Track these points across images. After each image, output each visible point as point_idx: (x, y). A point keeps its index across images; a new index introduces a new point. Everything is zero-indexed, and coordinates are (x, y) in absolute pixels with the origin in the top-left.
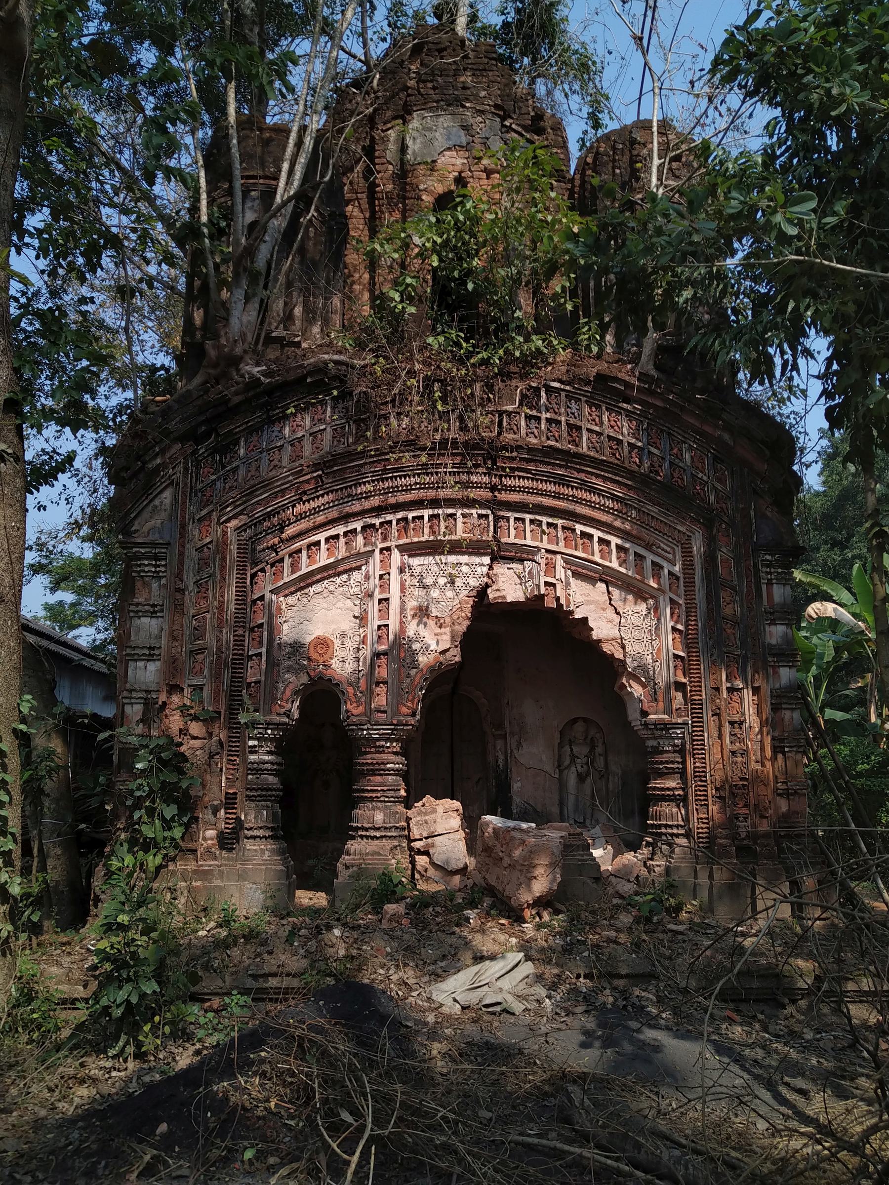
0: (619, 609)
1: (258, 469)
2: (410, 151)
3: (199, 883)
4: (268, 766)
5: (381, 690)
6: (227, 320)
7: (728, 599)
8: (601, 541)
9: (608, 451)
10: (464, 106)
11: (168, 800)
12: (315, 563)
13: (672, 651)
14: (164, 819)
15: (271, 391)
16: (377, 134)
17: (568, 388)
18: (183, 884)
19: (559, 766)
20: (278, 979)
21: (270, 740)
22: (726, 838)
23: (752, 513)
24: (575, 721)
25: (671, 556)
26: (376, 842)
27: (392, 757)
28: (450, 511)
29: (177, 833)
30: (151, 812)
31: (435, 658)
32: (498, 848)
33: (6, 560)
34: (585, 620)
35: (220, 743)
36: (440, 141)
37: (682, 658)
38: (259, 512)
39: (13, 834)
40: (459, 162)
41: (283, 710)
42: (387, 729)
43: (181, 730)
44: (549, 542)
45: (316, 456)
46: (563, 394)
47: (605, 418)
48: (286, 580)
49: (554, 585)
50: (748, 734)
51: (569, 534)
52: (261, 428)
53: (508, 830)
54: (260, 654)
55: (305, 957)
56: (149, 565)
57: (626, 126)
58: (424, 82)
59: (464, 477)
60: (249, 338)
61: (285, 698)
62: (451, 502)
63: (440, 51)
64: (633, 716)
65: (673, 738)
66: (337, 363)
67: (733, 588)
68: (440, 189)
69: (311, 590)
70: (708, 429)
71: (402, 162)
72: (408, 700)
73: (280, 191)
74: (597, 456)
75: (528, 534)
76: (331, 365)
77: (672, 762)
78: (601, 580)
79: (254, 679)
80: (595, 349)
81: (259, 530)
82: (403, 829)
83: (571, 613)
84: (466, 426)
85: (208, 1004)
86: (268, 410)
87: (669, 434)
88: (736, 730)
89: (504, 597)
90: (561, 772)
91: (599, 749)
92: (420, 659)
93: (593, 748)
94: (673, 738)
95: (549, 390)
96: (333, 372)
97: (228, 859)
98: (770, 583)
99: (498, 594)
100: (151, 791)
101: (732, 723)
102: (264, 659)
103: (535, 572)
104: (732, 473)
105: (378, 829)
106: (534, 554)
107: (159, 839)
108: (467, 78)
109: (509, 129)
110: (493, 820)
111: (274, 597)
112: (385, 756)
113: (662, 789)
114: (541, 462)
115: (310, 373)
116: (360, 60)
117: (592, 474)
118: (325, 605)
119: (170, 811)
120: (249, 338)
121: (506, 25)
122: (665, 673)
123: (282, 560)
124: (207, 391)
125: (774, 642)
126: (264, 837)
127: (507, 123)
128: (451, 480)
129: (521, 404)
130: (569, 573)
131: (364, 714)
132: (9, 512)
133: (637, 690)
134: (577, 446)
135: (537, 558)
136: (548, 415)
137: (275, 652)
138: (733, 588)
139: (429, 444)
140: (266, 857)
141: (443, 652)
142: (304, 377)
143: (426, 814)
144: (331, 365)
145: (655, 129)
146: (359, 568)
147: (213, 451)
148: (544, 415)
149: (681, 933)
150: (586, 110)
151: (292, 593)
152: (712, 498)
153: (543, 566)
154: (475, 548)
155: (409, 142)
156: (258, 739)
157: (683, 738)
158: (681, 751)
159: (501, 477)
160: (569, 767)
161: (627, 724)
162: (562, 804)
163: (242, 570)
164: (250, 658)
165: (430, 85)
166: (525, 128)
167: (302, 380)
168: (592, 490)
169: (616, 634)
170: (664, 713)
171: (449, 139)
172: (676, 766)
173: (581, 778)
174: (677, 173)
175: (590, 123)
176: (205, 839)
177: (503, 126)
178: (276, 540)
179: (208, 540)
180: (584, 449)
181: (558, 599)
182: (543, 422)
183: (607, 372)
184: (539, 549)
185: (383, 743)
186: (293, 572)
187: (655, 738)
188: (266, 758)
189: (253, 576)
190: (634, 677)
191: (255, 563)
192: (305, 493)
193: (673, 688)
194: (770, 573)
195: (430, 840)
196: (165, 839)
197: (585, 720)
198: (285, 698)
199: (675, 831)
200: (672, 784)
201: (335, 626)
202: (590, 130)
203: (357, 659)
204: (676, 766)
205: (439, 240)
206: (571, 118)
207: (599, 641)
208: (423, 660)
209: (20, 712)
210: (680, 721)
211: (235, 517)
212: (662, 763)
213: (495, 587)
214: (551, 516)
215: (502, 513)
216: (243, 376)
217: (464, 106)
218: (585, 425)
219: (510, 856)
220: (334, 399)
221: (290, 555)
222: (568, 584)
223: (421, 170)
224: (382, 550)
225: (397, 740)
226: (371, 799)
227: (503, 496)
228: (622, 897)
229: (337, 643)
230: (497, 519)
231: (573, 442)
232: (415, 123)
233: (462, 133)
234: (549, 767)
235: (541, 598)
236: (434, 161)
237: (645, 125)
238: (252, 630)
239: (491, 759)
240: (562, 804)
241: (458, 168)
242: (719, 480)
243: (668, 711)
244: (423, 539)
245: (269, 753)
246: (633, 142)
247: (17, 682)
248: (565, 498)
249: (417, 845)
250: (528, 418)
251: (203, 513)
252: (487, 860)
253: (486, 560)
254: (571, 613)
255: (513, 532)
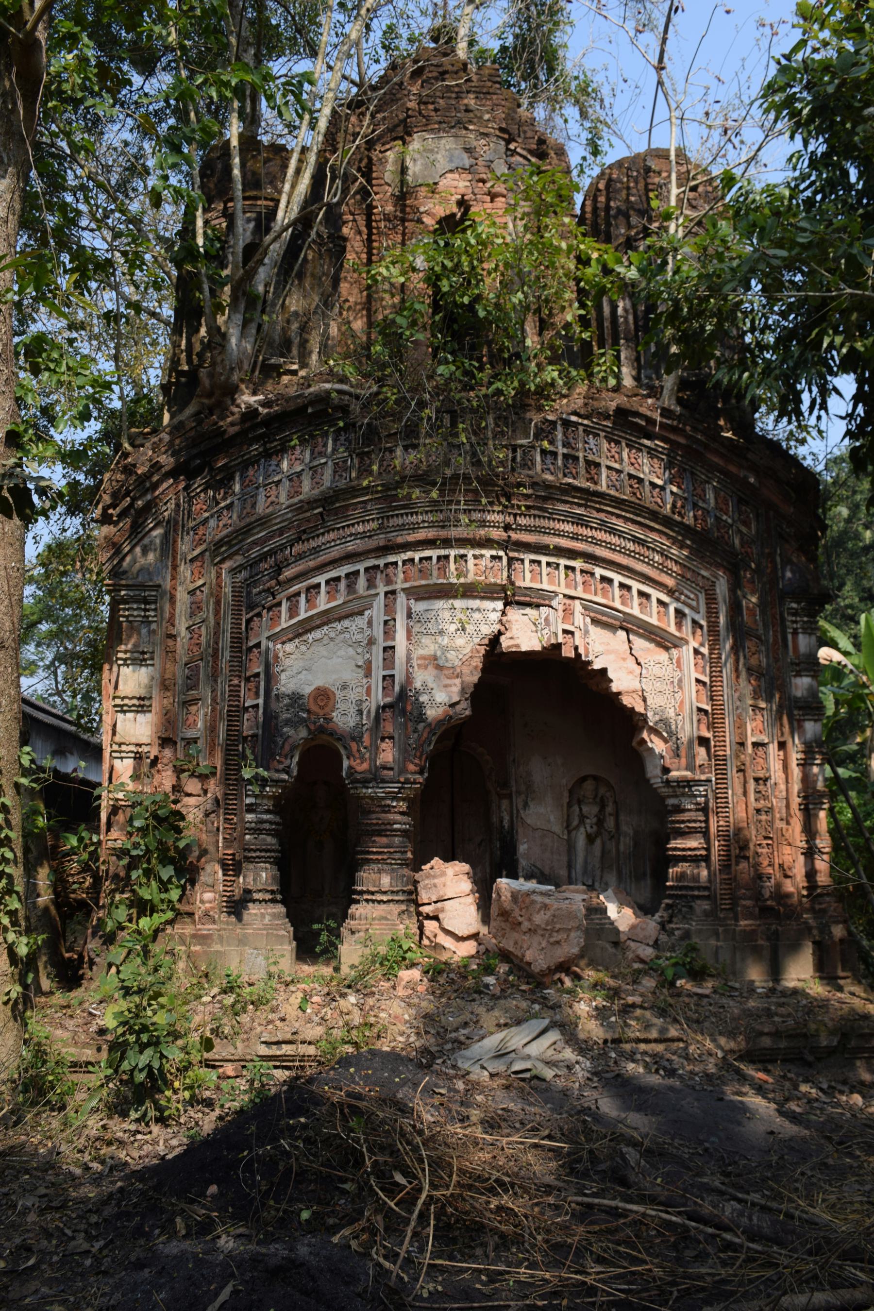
0: (640, 660)
1: (254, 505)
2: (410, 172)
3: (198, 948)
4: (267, 826)
5: (387, 745)
6: (223, 347)
7: (753, 649)
8: (622, 586)
9: (628, 490)
10: (466, 129)
11: (164, 860)
12: (315, 607)
13: (696, 704)
14: (161, 881)
15: (269, 421)
17: (586, 422)
18: (183, 948)
19: (567, 827)
21: (269, 797)
22: (750, 898)
23: (778, 559)
24: (584, 779)
25: (694, 603)
27: (398, 817)
28: (462, 551)
29: (175, 894)
30: (148, 873)
32: (517, 913)
33: (6, 603)
34: (604, 671)
35: (217, 800)
36: (442, 163)
37: (706, 712)
38: (254, 553)
39: (17, 893)
41: (281, 767)
43: (174, 787)
45: (316, 492)
46: (581, 428)
47: (625, 455)
49: (572, 633)
50: (773, 791)
51: (587, 577)
52: (257, 462)
53: (528, 894)
54: (256, 706)
56: (138, 609)
58: (426, 103)
59: (477, 516)
60: (246, 366)
61: (284, 752)
62: (463, 542)
64: (653, 772)
65: (695, 796)
66: (339, 392)
68: (441, 211)
69: (310, 637)
70: (733, 469)
71: (403, 182)
72: (415, 756)
73: (280, 214)
74: (617, 494)
75: (545, 578)
77: (695, 821)
78: (622, 628)
79: (250, 733)
80: (612, 382)
81: (254, 571)
84: (479, 461)
85: (221, 1070)
86: (265, 444)
87: (692, 473)
88: (761, 787)
89: (518, 646)
90: (569, 832)
91: (610, 809)
92: (429, 712)
93: (603, 807)
94: (695, 796)
95: (567, 424)
96: (336, 401)
97: (228, 923)
98: (795, 633)
99: (511, 642)
100: (148, 851)
101: (757, 780)
102: (261, 711)
103: (551, 618)
104: (757, 516)
105: (385, 893)
106: (551, 599)
107: (156, 901)
108: (470, 101)
109: (514, 152)
110: (503, 883)
111: (271, 645)
112: (391, 816)
113: (684, 850)
115: (311, 403)
116: (353, 82)
118: (325, 653)
119: (166, 873)
120: (246, 366)
121: (504, 49)
123: (279, 604)
124: (200, 423)
125: (799, 694)
127: (512, 146)
128: (464, 519)
129: (537, 437)
130: (588, 620)
133: (658, 745)
134: (596, 483)
135: (554, 603)
136: (565, 451)
137: (274, 705)
140: (267, 920)
141: (453, 705)
142: (305, 407)
146: (361, 613)
148: (561, 450)
149: (707, 996)
150: (585, 135)
151: (290, 640)
152: (737, 542)
154: (489, 592)
155: (408, 162)
156: (256, 796)
157: (706, 796)
158: (705, 810)
159: (515, 515)
160: (577, 827)
161: (644, 781)
162: (570, 866)
164: (246, 709)
165: (431, 107)
166: (530, 152)
168: (612, 531)
169: (637, 686)
170: (687, 769)
171: (451, 161)
172: (697, 825)
173: (590, 839)
174: (694, 203)
177: (508, 149)
179: (201, 582)
180: (603, 487)
181: (576, 648)
182: (560, 458)
184: (556, 594)
186: (291, 617)
187: (676, 796)
189: (248, 621)
190: (654, 731)
192: (304, 531)
193: (696, 743)
194: (796, 622)
195: (439, 905)
196: (162, 901)
197: (595, 778)
198: (284, 752)
199: (696, 893)
201: (334, 677)
203: (360, 712)
204: (697, 825)
206: (572, 144)
207: (619, 693)
208: (431, 713)
209: (21, 765)
210: (703, 777)
211: (229, 557)
212: (683, 822)
214: (569, 558)
215: (515, 554)
216: (238, 406)
217: (466, 129)
218: (604, 462)
219: (530, 920)
222: (587, 632)
223: (423, 192)
224: (386, 593)
225: (403, 799)
226: (377, 861)
227: (515, 536)
228: (642, 961)
229: (339, 695)
230: (511, 560)
231: (591, 479)
232: (416, 144)
233: (465, 156)
234: (557, 828)
235: (558, 647)
236: (436, 184)
237: (662, 155)
238: (248, 680)
239: (495, 819)
240: (570, 866)
243: (690, 767)
244: (430, 582)
246: (648, 170)
247: (16, 734)
248: (584, 539)
249: (425, 909)
250: (544, 452)
251: (196, 553)
252: (503, 925)
253: (499, 605)
254: (589, 663)
255: (528, 575)
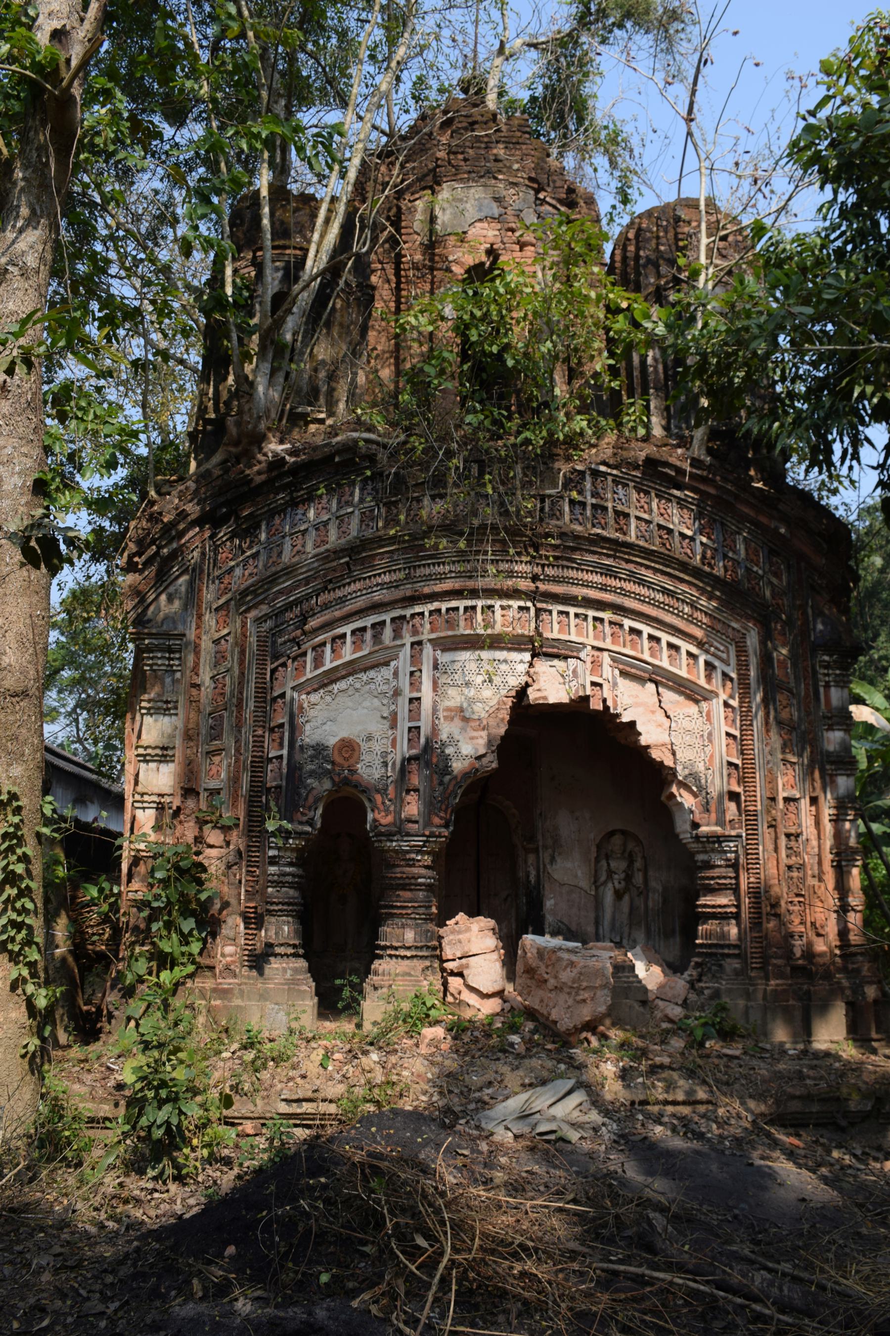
0: (669, 713)
1: (280, 554)
2: (439, 221)
3: (218, 1002)
4: (289, 879)
5: (412, 798)
6: (251, 395)
7: (785, 702)
8: (651, 637)
9: (658, 541)
10: (496, 178)
11: (186, 913)
12: (340, 657)
13: (726, 758)
14: (182, 933)
15: (295, 470)
16: (404, 204)
17: (615, 472)
20: (314, 1105)
21: (292, 850)
24: (612, 834)
25: (724, 656)
26: (406, 962)
27: (423, 871)
29: (195, 947)
30: (168, 925)
31: (471, 764)
32: (543, 969)
34: (633, 724)
35: (239, 852)
38: (280, 602)
39: (37, 944)
40: (491, 233)
41: (305, 819)
42: (418, 841)
43: (196, 838)
44: (596, 638)
46: (610, 478)
47: (654, 505)
48: (309, 675)
49: (600, 685)
51: (616, 629)
52: (284, 511)
54: (280, 757)
55: (341, 1082)
56: (162, 658)
57: (668, 204)
58: (455, 153)
59: (504, 566)
60: (273, 415)
63: (472, 124)
64: (682, 828)
65: (726, 852)
66: (367, 441)
67: (790, 691)
68: (470, 260)
69: (336, 687)
70: (764, 520)
71: (432, 231)
72: (440, 809)
74: (646, 545)
75: (573, 629)
76: (361, 443)
77: (725, 878)
78: (651, 680)
80: (641, 432)
82: (434, 948)
83: (618, 716)
84: (507, 511)
85: (240, 1128)
86: (291, 493)
87: (722, 524)
89: (545, 698)
90: (597, 888)
91: (638, 864)
93: (631, 862)
94: (726, 852)
95: (595, 474)
96: (363, 451)
97: (249, 977)
98: (827, 686)
99: (538, 694)
100: (169, 903)
101: (788, 836)
102: (285, 762)
103: (580, 670)
104: (789, 567)
105: (409, 948)
106: (579, 650)
107: (177, 954)
108: (500, 151)
109: (543, 202)
111: (295, 695)
112: (415, 870)
113: (713, 907)
114: (587, 551)
115: (338, 452)
116: (383, 132)
117: (641, 565)
118: (350, 704)
119: (188, 925)
120: (273, 415)
121: (533, 99)
122: (717, 781)
123: (304, 654)
125: (831, 748)
126: (286, 955)
127: (541, 196)
128: (492, 569)
129: (565, 486)
130: (617, 672)
131: (394, 824)
132: (35, 598)
133: (687, 800)
134: (625, 534)
135: (582, 655)
136: (594, 501)
138: (790, 691)
139: (467, 530)
141: (479, 758)
142: (331, 457)
143: (459, 932)
144: (361, 443)
145: (702, 207)
146: (387, 664)
147: (233, 536)
148: (590, 500)
149: (737, 1058)
150: (615, 184)
151: (315, 690)
152: (768, 593)
153: (589, 665)
154: (517, 643)
155: (438, 212)
156: (279, 849)
158: (735, 866)
159: (543, 566)
160: (605, 883)
162: (597, 923)
163: (262, 664)
164: (270, 760)
165: (460, 157)
166: (560, 201)
167: (330, 458)
168: (642, 582)
169: (666, 739)
170: (717, 824)
171: (480, 210)
172: (728, 881)
173: (618, 895)
174: (724, 252)
175: (619, 197)
176: (223, 955)
177: (537, 199)
178: (299, 632)
180: (632, 537)
181: (604, 701)
182: (589, 508)
183: (657, 456)
184: (584, 645)
185: (413, 856)
186: (316, 668)
187: (706, 852)
188: (288, 869)
189: (273, 671)
190: (683, 785)
191: (275, 657)
192: (330, 581)
193: (726, 797)
194: (828, 675)
195: (464, 961)
196: (183, 954)
197: (623, 832)
200: (723, 901)
201: (359, 728)
202: (618, 205)
203: (385, 764)
204: (728, 881)
205: (478, 314)
206: (602, 192)
208: (457, 766)
209: (43, 814)
210: (733, 833)
211: (255, 606)
212: (713, 878)
213: (535, 686)
214: (597, 609)
216: (265, 455)
217: (496, 178)
218: (633, 512)
219: (556, 977)
220: (365, 481)
221: (314, 649)
222: (615, 684)
224: (413, 644)
225: (428, 853)
226: (401, 916)
228: (671, 1021)
230: (538, 611)
231: (620, 530)
233: (495, 205)
235: (586, 699)
237: (692, 204)
238: (272, 730)
240: (597, 923)
241: (491, 240)
242: (777, 575)
243: (720, 822)
245: (291, 864)
246: (678, 219)
248: (613, 590)
249: (449, 966)
250: (572, 502)
251: (221, 602)
252: (529, 982)
253: (527, 656)
254: (618, 716)
255: (556, 627)
